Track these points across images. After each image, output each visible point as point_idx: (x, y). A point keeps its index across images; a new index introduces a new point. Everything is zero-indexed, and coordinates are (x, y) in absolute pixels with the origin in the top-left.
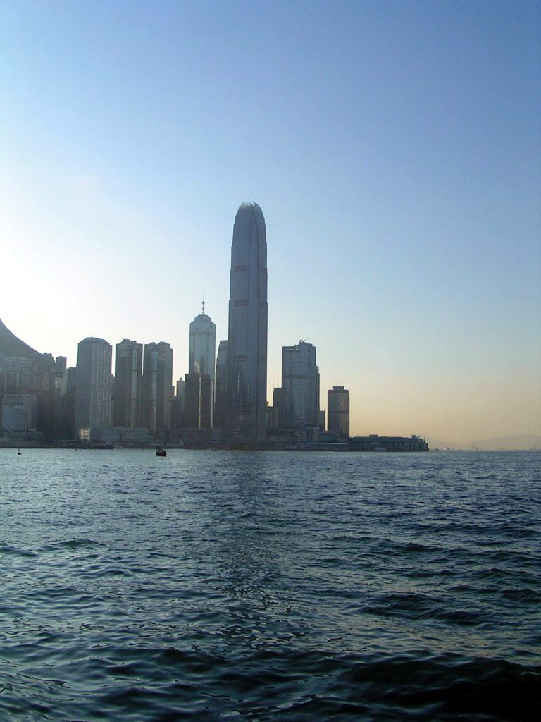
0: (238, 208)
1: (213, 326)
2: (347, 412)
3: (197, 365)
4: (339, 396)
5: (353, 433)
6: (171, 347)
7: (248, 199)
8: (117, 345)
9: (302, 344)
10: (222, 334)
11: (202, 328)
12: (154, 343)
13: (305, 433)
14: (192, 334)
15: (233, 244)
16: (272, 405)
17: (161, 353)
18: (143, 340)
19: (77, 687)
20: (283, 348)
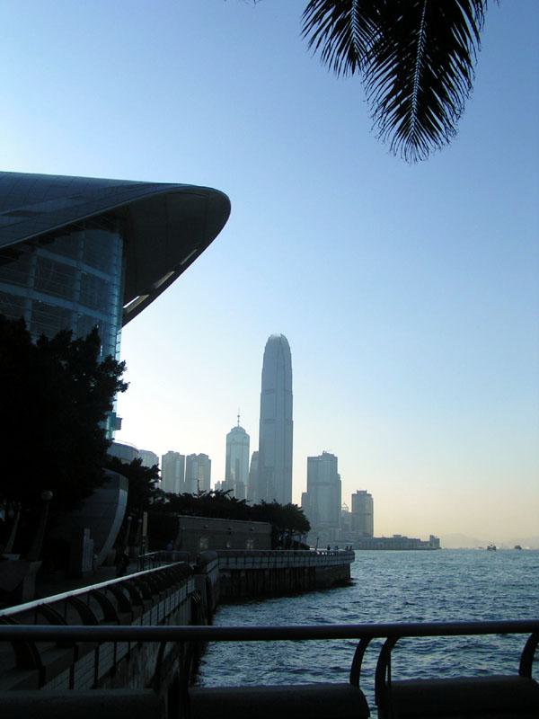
0: (266, 341)
1: (247, 437)
2: (371, 514)
3: (233, 471)
4: (362, 499)
5: (377, 533)
6: (197, 454)
7: (277, 333)
8: (163, 456)
9: (325, 455)
10: (254, 446)
11: (237, 438)
12: (195, 455)
13: (327, 534)
14: (228, 445)
15: (291, 370)
16: (18, 556)
17: (202, 461)
18: (186, 451)
19: (428, 650)
20: (309, 458)
